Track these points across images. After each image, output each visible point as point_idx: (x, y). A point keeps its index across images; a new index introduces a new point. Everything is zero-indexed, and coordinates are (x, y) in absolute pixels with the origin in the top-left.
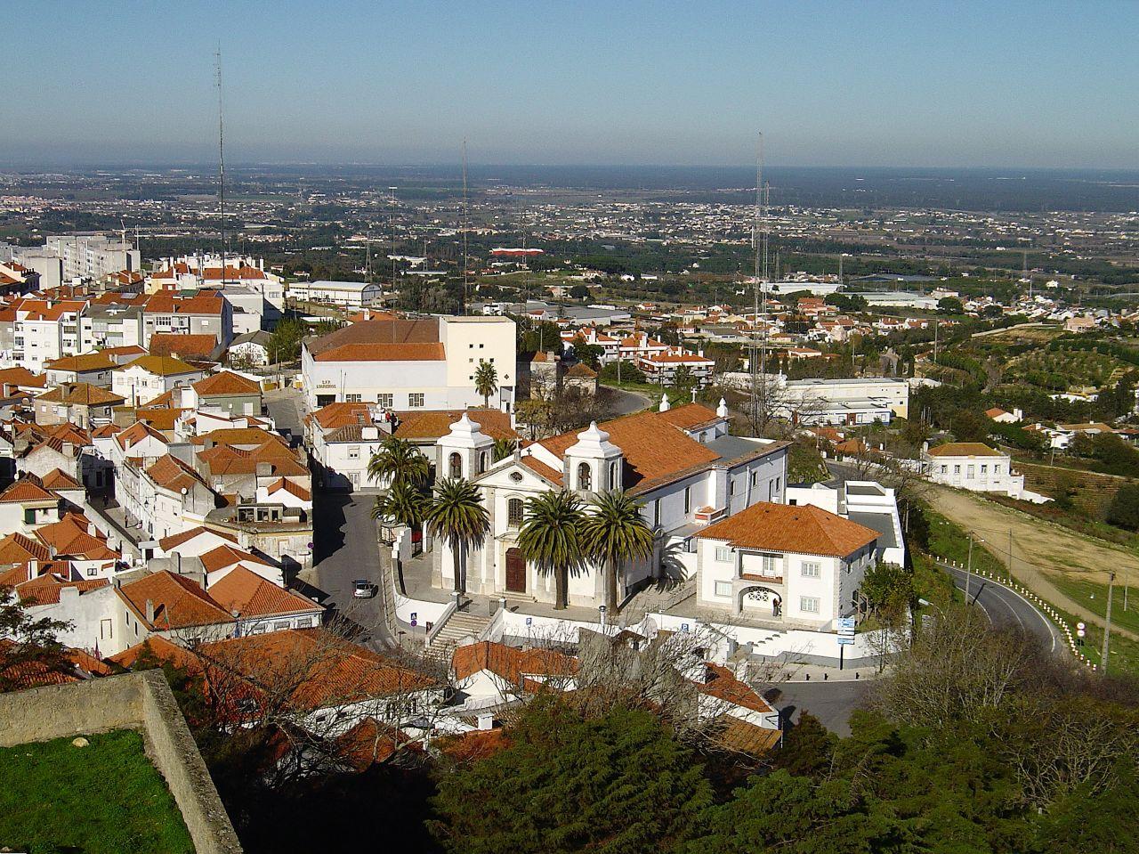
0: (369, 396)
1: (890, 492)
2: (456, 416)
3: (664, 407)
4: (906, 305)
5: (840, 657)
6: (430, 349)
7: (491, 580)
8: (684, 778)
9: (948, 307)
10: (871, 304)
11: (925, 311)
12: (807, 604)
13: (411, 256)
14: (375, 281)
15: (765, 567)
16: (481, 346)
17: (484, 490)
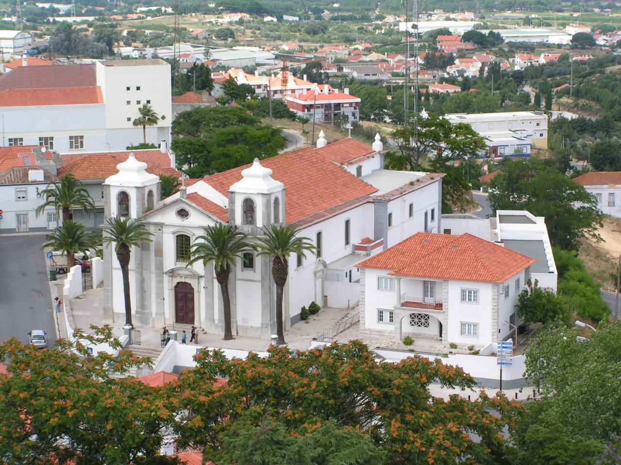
0: (31, 140)
1: (540, 221)
2: (119, 158)
3: (321, 142)
4: (540, 41)
5: (499, 379)
6: (85, 90)
7: (161, 313)
8: (162, 401)
9: (582, 42)
10: (507, 41)
11: (559, 46)
12: (467, 328)
13: (58, 3)
14: (25, 28)
15: (425, 295)
16: (138, 88)
17: (152, 229)
